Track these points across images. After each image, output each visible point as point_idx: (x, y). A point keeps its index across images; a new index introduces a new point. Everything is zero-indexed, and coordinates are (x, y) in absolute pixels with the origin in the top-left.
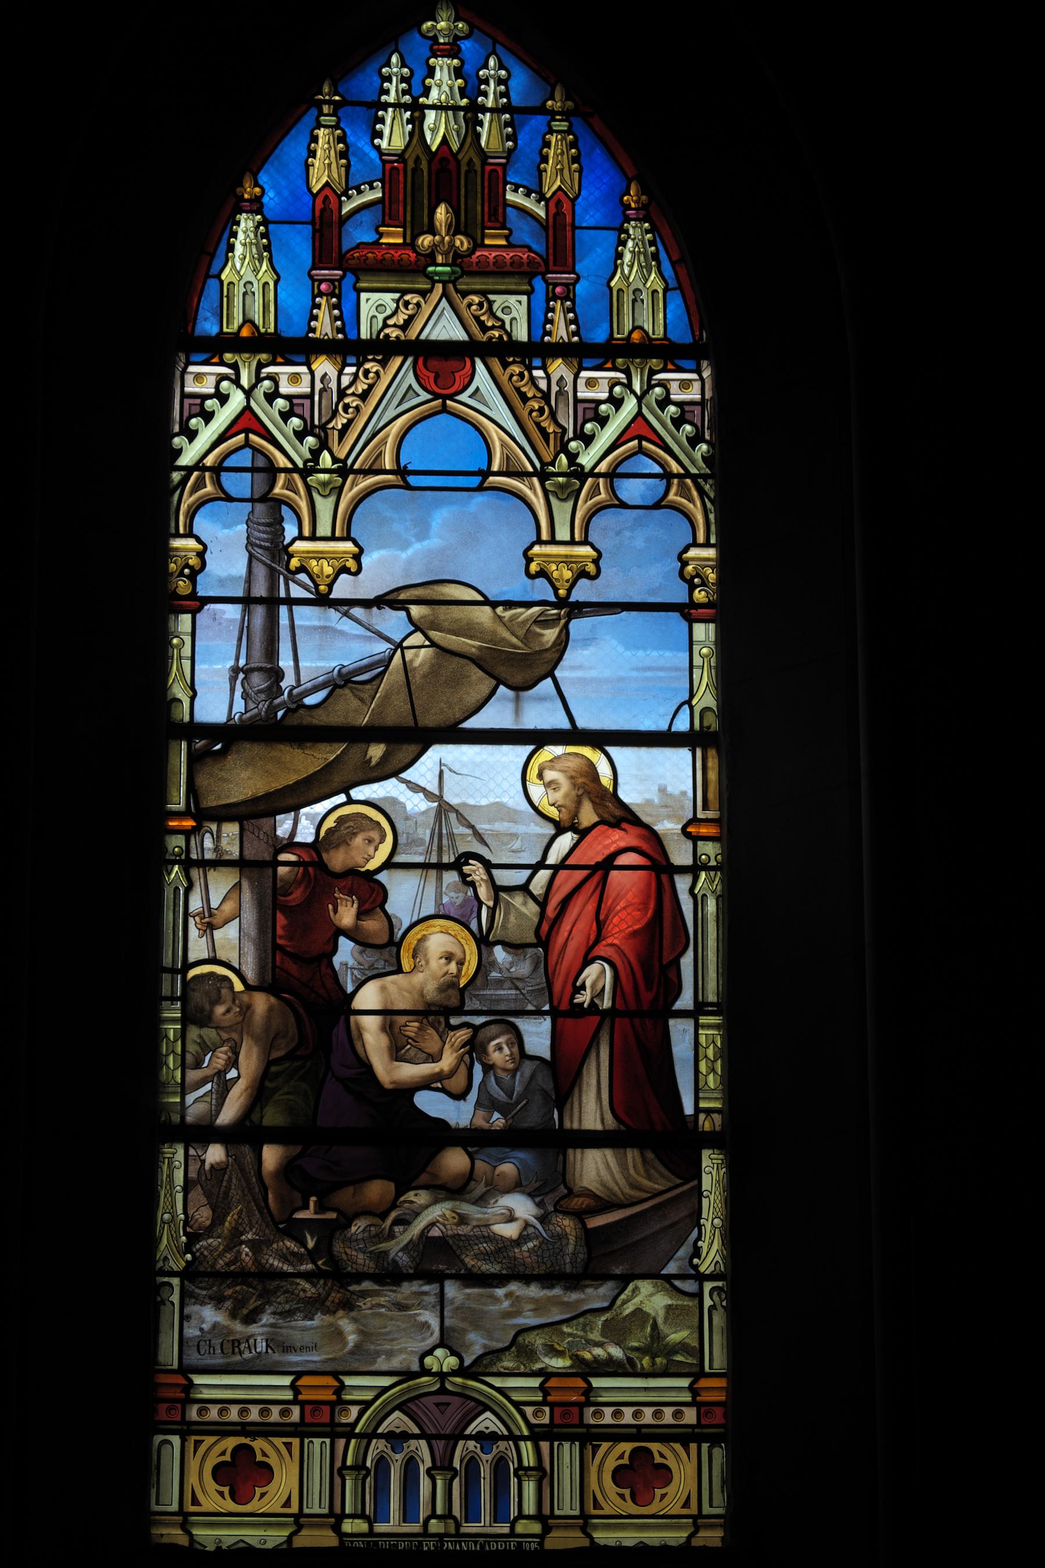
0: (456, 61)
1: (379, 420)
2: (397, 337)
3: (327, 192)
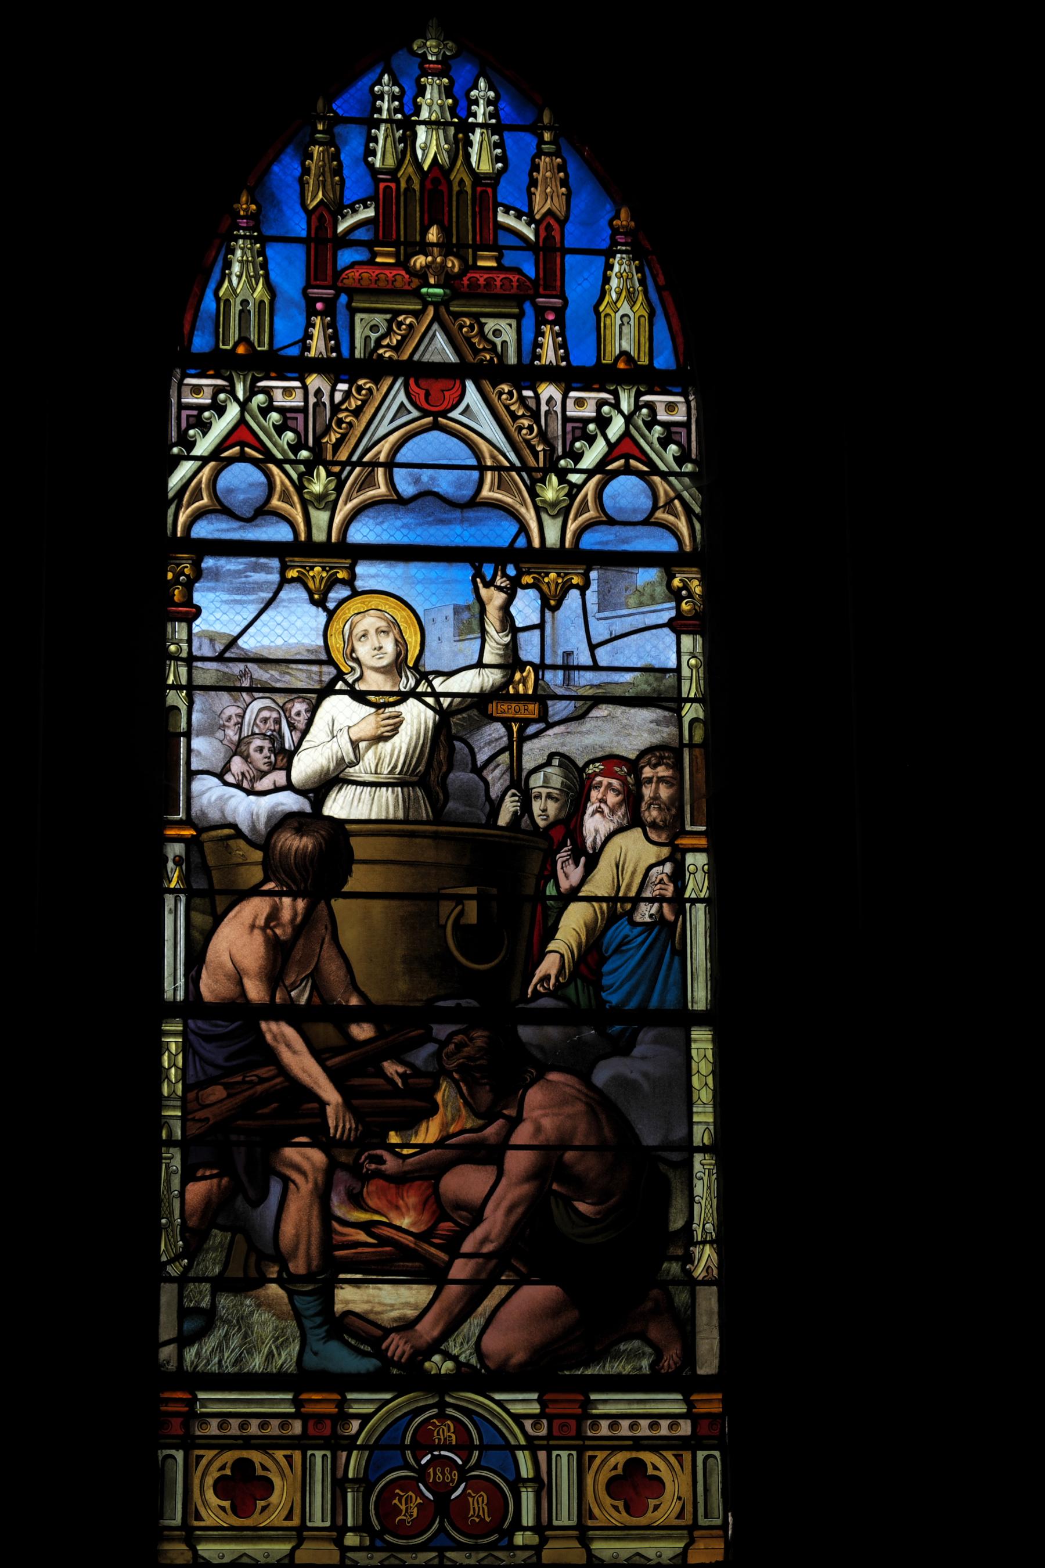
0: (445, 80)
1: (373, 435)
2: (390, 357)
3: (321, 209)
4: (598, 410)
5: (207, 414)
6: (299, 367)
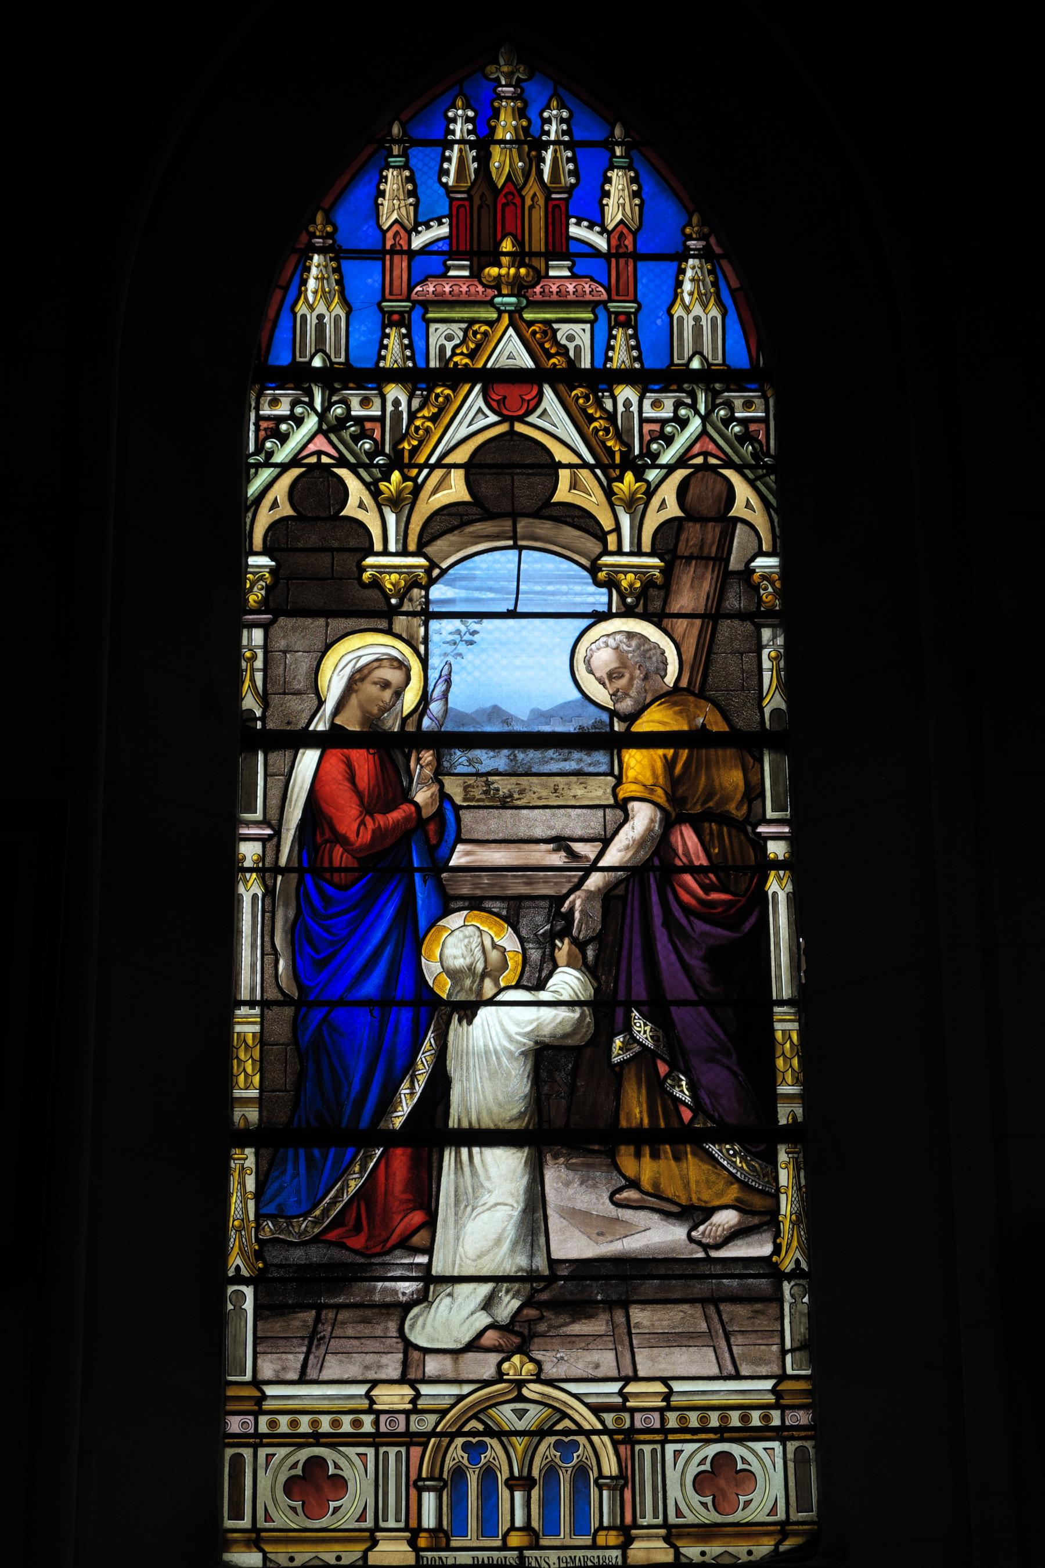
4: (675, 411)
5: (284, 427)
6: (376, 378)
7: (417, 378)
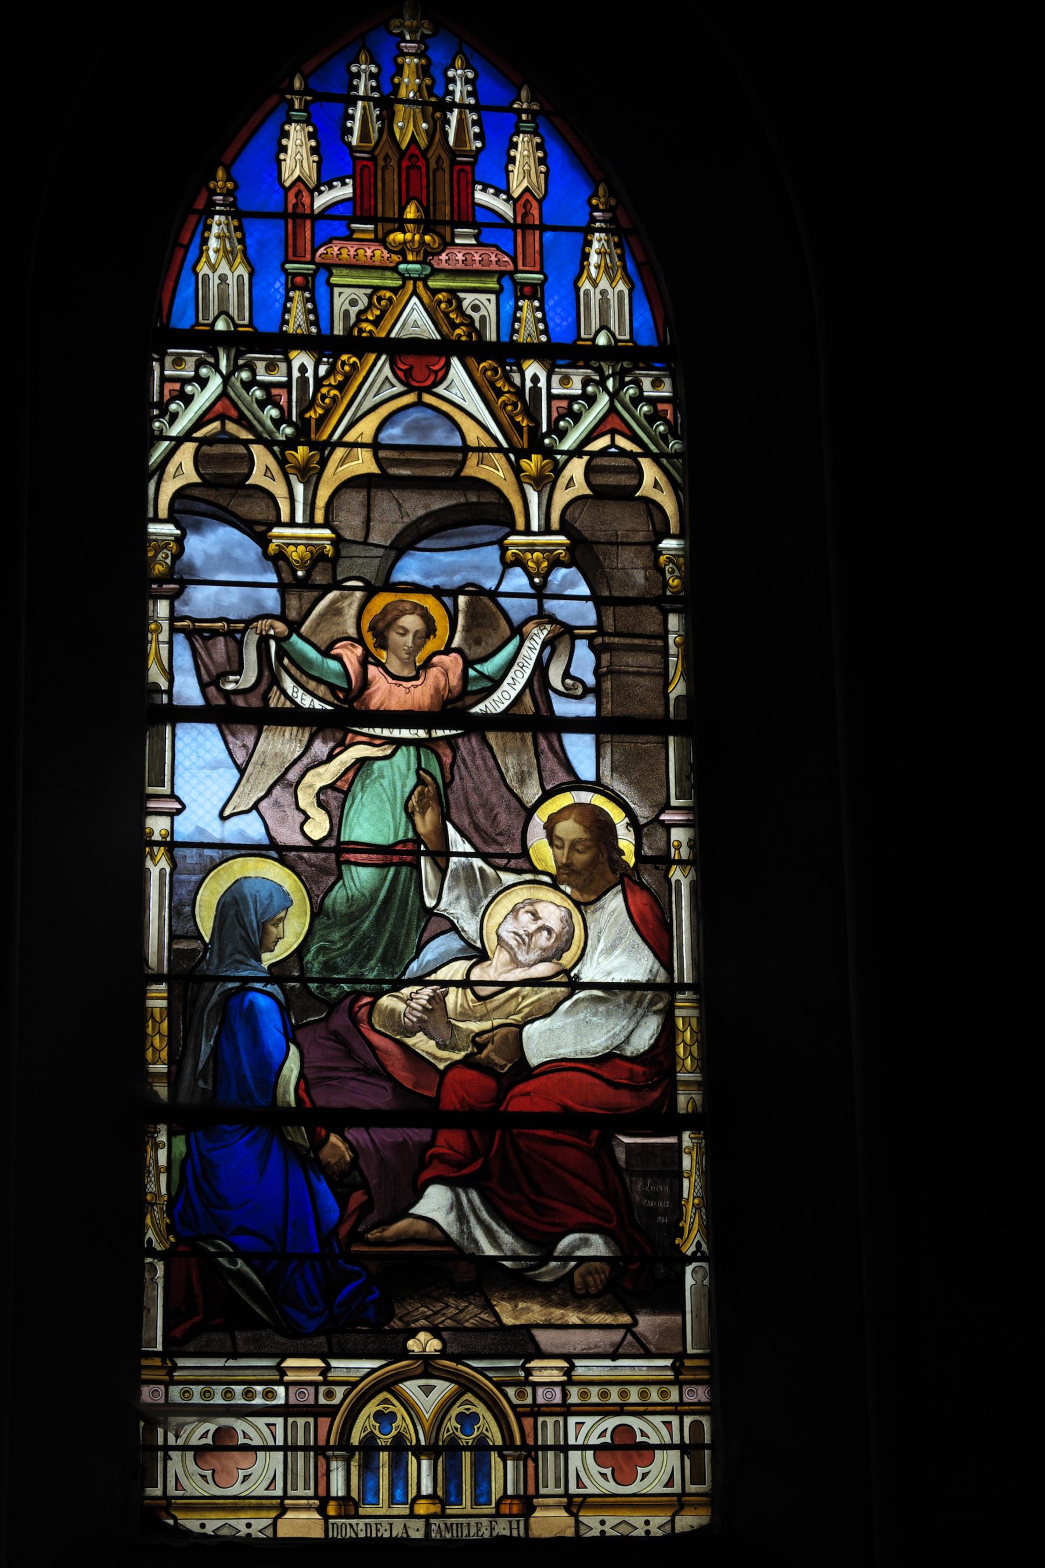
5: (189, 389)
6: (282, 344)
7: (322, 345)
